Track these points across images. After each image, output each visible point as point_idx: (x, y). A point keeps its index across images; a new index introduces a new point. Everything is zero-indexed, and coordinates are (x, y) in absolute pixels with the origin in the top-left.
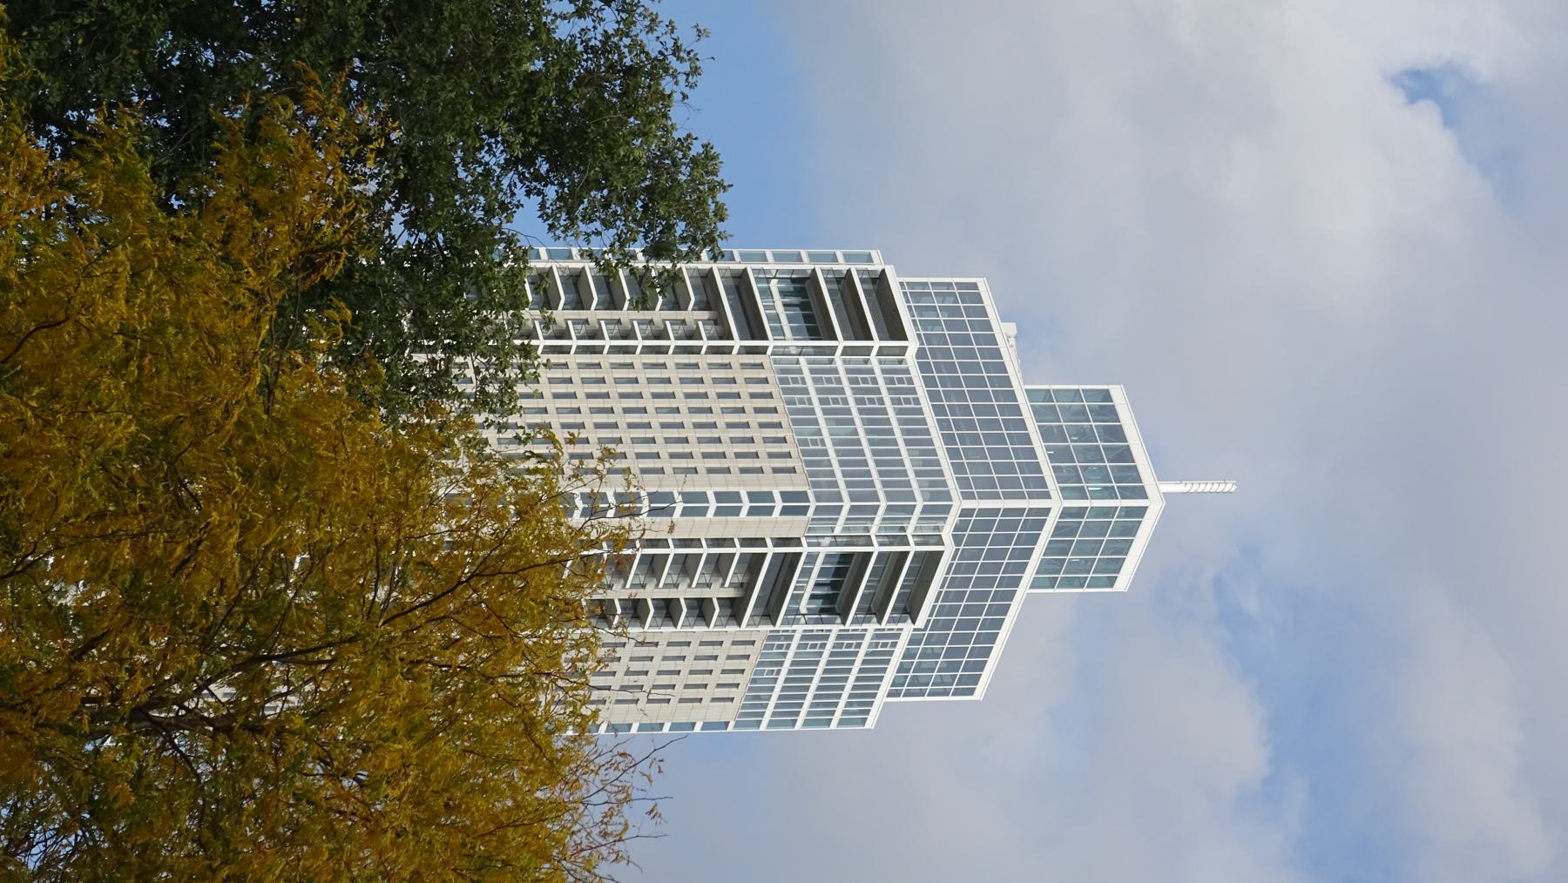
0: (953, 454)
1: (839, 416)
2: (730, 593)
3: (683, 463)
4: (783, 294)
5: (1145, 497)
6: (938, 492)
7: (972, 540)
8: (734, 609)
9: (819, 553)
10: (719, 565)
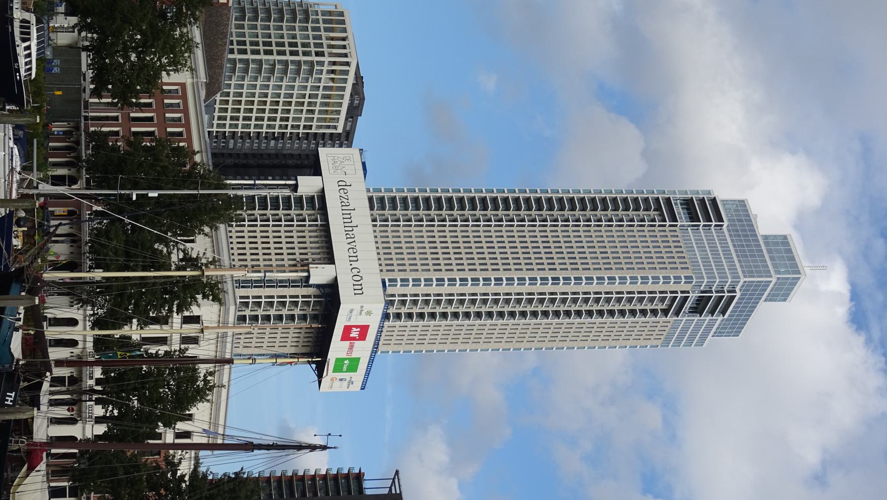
0: (740, 261)
1: (702, 249)
2: (664, 307)
3: (651, 266)
4: (681, 204)
5: (800, 273)
6: (736, 276)
7: (745, 290)
8: (665, 312)
9: (693, 296)
10: (662, 300)
